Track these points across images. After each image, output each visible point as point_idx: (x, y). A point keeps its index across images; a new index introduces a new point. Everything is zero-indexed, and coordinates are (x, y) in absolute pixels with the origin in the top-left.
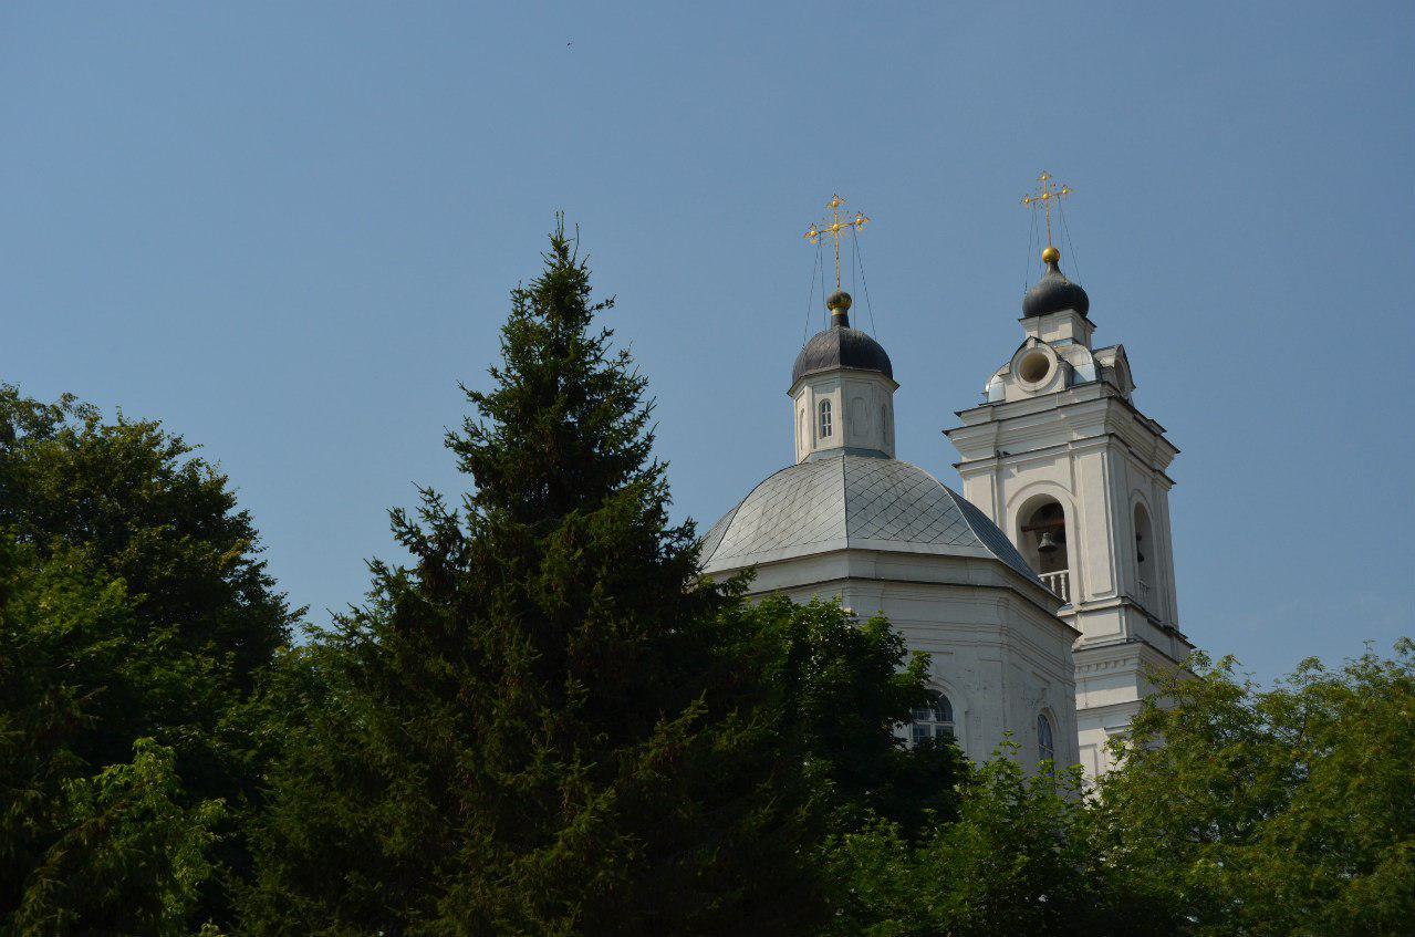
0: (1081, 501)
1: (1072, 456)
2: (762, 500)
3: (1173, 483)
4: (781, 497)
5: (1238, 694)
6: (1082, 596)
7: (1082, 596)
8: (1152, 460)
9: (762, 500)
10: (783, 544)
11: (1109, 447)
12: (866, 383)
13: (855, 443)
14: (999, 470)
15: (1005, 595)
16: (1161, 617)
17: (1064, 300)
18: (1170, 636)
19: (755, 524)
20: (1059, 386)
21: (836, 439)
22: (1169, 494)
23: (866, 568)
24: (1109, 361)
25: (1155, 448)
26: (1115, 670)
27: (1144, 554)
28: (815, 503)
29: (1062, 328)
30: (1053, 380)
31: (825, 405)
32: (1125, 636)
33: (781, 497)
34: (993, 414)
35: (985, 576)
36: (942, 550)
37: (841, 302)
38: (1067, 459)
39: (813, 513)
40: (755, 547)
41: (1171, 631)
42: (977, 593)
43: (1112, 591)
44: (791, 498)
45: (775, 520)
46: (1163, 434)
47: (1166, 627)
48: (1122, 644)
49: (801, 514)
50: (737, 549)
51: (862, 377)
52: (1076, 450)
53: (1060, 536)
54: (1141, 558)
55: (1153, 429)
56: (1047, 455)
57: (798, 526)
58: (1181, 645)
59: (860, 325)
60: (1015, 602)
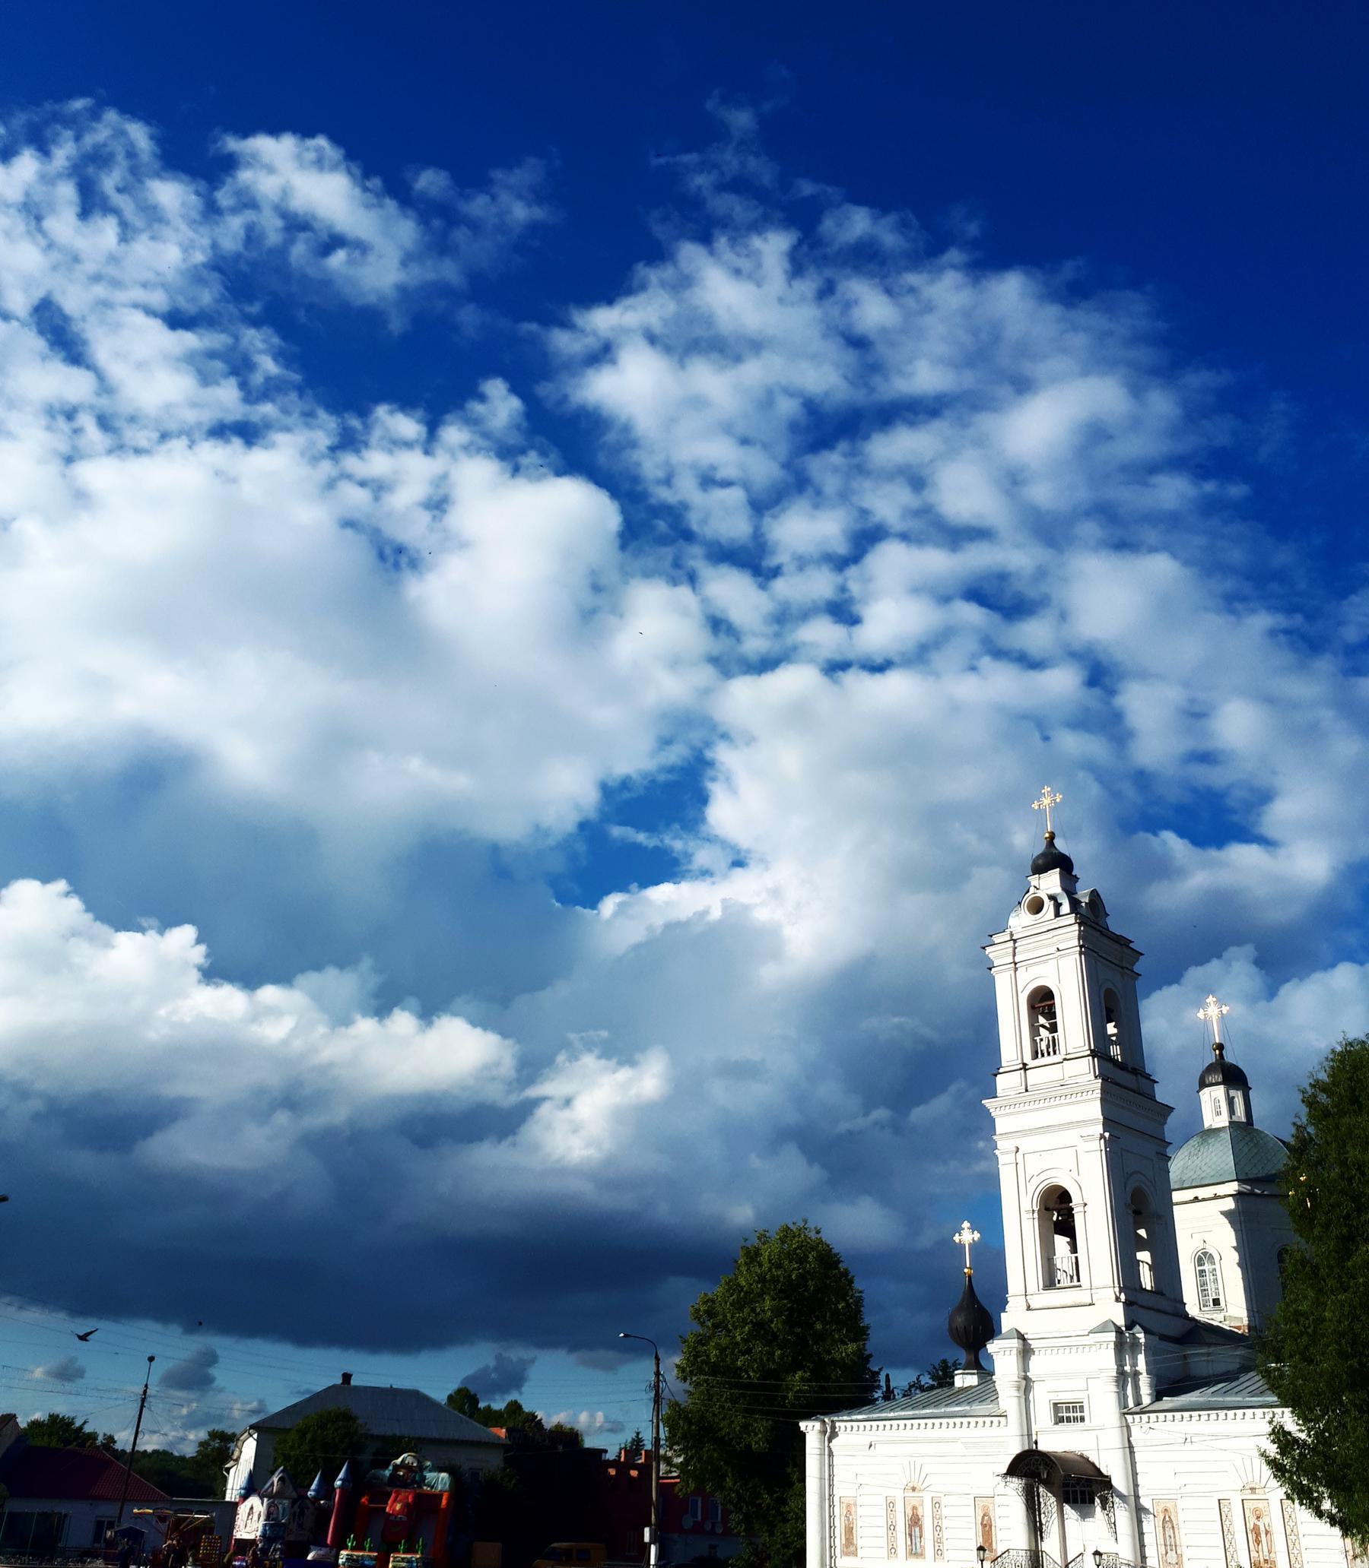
55: (1123, 942)
58: (1144, 1081)
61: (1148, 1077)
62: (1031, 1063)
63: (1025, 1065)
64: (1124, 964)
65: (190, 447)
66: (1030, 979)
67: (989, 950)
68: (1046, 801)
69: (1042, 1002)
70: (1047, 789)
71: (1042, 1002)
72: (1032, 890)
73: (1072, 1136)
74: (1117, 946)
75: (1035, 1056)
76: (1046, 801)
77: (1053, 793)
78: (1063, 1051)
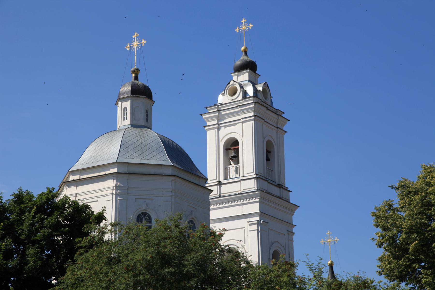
0: (244, 139)
1: (243, 123)
2: (96, 144)
3: (286, 132)
4: (102, 143)
5: (94, 212)
6: (243, 174)
7: (243, 174)
8: (277, 124)
9: (96, 144)
10: (98, 160)
11: (255, 120)
12: (142, 101)
13: (135, 123)
14: (219, 129)
15: (174, 178)
16: (277, 180)
17: (250, 66)
18: (280, 188)
19: (91, 153)
20: (240, 97)
21: (128, 122)
22: (284, 136)
23: (124, 169)
24: (260, 88)
25: (278, 119)
26: (243, 202)
27: (270, 157)
28: (111, 145)
29: (245, 76)
30: (239, 96)
31: (125, 109)
32: (256, 188)
33: (102, 143)
34: (217, 108)
35: (168, 171)
36: (152, 162)
37: (136, 72)
38: (241, 124)
39: (110, 149)
40: (89, 161)
41: (280, 186)
42: (165, 178)
43: (253, 172)
44: (105, 143)
45: (98, 151)
46: (283, 115)
47: (279, 185)
48: (254, 192)
49: (106, 149)
50: (84, 162)
51: (139, 99)
52: (244, 121)
53: (237, 151)
54: (268, 160)
55: (278, 113)
56: (233, 123)
57: (104, 153)
58: (284, 191)
59: (141, 81)
60: (179, 180)
61: (286, 189)
62: (223, 182)
63: (220, 182)
64: (279, 126)
65: (403, 186)
66: (226, 133)
67: (204, 116)
68: (135, 44)
69: (232, 148)
70: (244, 21)
71: (232, 148)
72: (232, 82)
73: (243, 222)
74: (276, 116)
75: (226, 178)
76: (135, 44)
77: (248, 23)
78: (241, 175)
